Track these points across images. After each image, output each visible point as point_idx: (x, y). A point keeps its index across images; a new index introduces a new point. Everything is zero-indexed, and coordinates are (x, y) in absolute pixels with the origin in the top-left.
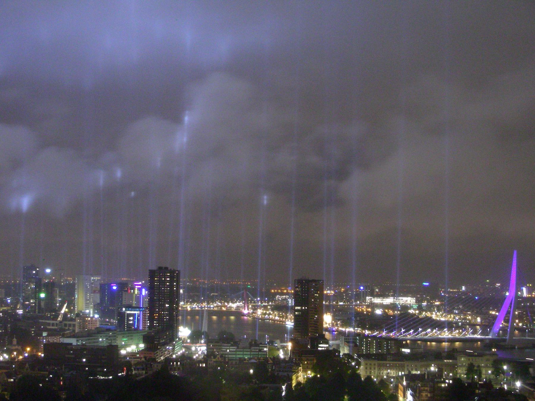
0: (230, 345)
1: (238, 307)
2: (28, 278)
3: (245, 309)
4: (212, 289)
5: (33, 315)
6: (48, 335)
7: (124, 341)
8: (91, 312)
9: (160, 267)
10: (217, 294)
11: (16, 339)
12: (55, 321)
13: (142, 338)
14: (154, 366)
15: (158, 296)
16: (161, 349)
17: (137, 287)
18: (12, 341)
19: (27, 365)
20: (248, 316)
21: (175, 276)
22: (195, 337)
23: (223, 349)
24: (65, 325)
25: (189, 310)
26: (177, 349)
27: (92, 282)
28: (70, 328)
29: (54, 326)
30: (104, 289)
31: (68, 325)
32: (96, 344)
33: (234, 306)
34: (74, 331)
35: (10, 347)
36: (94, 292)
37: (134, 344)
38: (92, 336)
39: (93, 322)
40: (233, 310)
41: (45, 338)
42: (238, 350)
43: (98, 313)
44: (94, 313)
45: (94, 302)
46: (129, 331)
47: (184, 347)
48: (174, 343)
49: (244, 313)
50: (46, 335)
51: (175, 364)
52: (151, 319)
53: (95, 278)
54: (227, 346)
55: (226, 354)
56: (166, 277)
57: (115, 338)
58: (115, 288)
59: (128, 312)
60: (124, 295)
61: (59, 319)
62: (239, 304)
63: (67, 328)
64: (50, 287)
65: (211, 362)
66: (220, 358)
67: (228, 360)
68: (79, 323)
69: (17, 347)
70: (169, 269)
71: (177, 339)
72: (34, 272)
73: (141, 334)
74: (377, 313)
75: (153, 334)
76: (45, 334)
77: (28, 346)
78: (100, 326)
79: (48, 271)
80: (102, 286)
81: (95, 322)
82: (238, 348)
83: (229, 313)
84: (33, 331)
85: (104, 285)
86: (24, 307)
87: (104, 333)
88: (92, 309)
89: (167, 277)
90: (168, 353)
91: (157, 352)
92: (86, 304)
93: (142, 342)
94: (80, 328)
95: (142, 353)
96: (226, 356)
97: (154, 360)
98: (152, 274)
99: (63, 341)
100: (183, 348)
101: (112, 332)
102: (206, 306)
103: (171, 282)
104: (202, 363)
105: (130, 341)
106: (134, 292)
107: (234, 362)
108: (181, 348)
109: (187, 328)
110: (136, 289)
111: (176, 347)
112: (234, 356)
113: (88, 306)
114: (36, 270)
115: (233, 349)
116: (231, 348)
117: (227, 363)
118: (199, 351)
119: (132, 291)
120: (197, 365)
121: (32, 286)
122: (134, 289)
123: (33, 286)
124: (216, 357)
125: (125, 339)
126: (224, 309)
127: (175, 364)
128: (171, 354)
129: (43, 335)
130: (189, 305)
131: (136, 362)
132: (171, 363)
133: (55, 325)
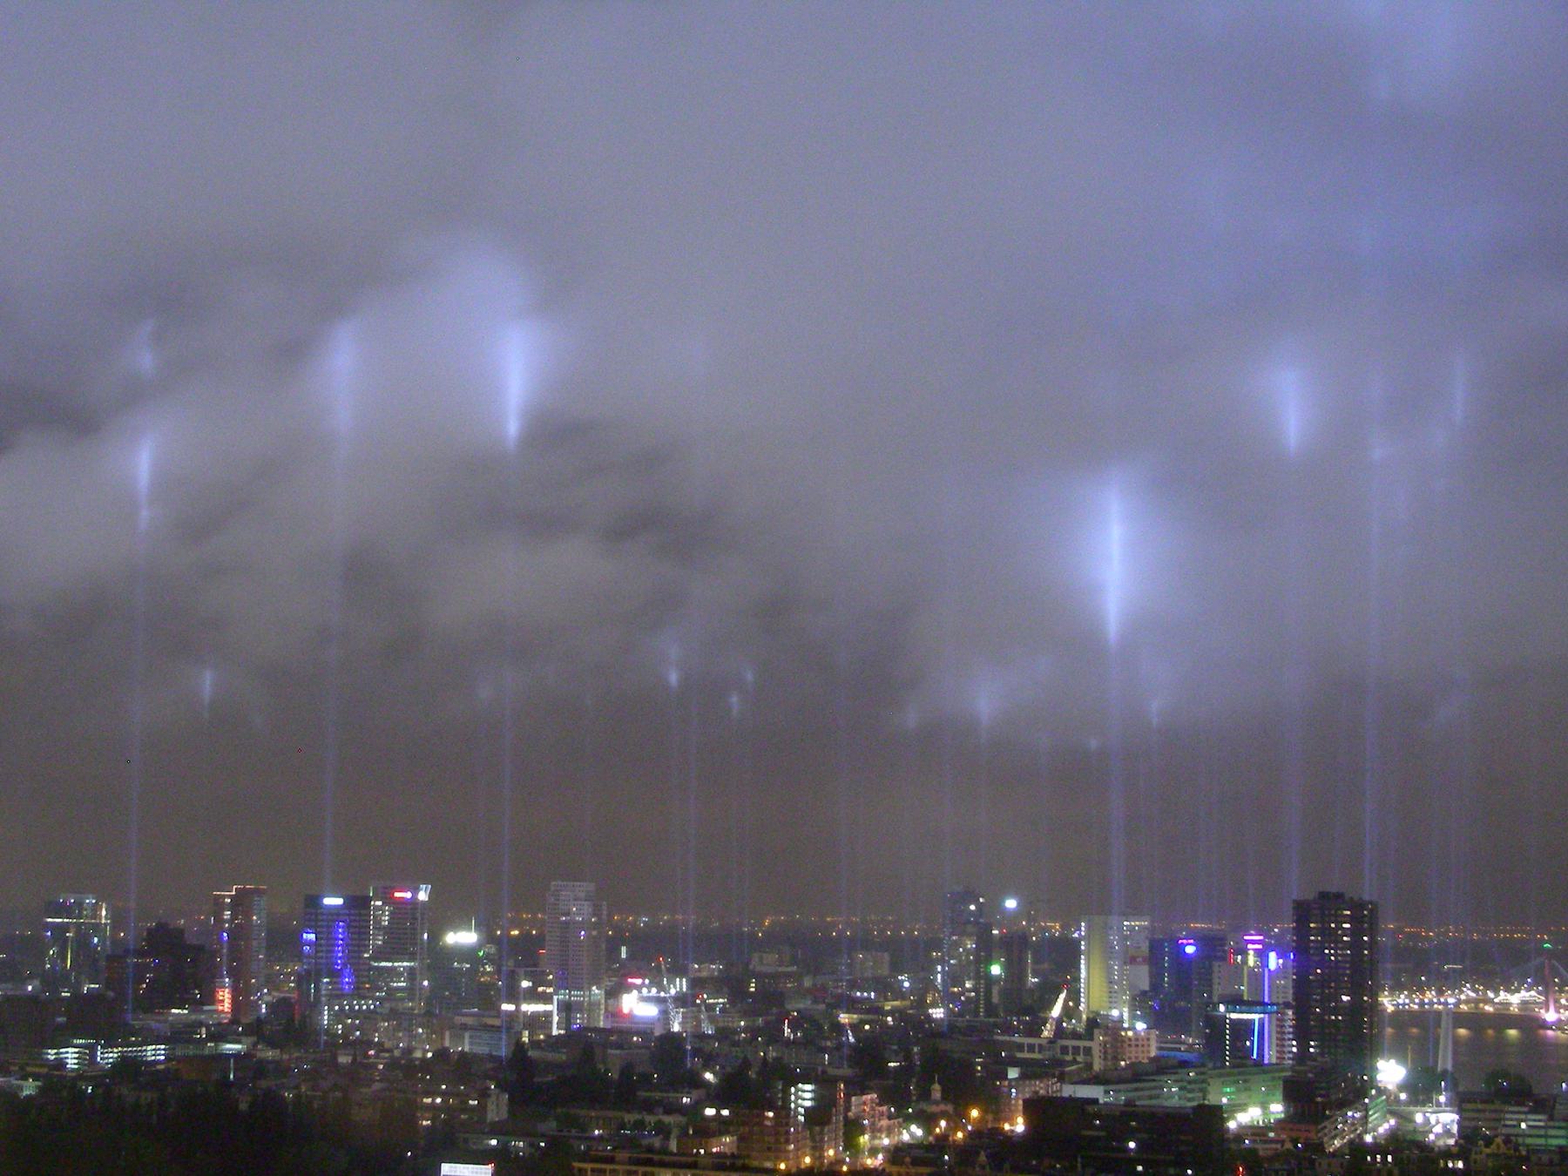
0: (1526, 1109)
1: (1524, 1003)
2: (960, 924)
3: (1547, 1010)
4: (1444, 953)
5: (974, 1021)
6: (1024, 1076)
7: (1225, 1094)
8: (1126, 1016)
9: (1323, 892)
10: (412, 964)
11: (939, 1083)
12: (1035, 1037)
13: (1281, 1086)
14: (1320, 1164)
15: (1341, 971)
16: (1332, 1120)
17: (1250, 946)
18: (930, 1091)
19: (982, 1158)
20: (1559, 1029)
21: (1364, 917)
22: (1421, 1088)
23: (1507, 1119)
24: (1064, 1050)
25: (1389, 1011)
26: (1375, 1119)
27: (1125, 933)
28: (1079, 1059)
29: (1074, 1047)
30: (1159, 951)
31: (1070, 1048)
32: (1154, 1102)
33: (1514, 999)
34: (1089, 1066)
35: (924, 1106)
36: (1132, 960)
37: (1255, 1104)
38: (1145, 1081)
39: (1140, 1043)
40: (1514, 1010)
41: (1013, 1083)
42: (1551, 1124)
43: (1142, 1018)
44: (1133, 1017)
45: (1131, 987)
46: (1238, 1067)
47: (1393, 1113)
48: (1367, 1101)
49: (1544, 1021)
50: (1017, 1076)
51: (1379, 1160)
52: (1302, 1034)
53: (1133, 924)
54: (1519, 1113)
55: (1516, 1136)
56: (1339, 919)
57: (1204, 1085)
58: (1190, 950)
59: (1234, 1016)
60: (1216, 969)
61: (1046, 1034)
62: (1528, 994)
63: (1069, 1058)
64: (1014, 947)
65: (1478, 1157)
66: (1502, 1145)
67: (1528, 1151)
68: (1103, 1045)
69: (942, 1107)
70: (1347, 897)
71: (1373, 1092)
72: (972, 907)
73: (1277, 1075)
74: (642, 1018)
75: (1310, 1075)
76: (1013, 1073)
77: (971, 1105)
78: (1158, 1052)
79: (1011, 904)
80: (1155, 947)
81: (1145, 1042)
82: (1551, 1118)
83: (1503, 1019)
84: (979, 1065)
85: (1160, 942)
86: (947, 998)
87: (1171, 1073)
88: (1127, 1006)
89: (1343, 919)
90: (1353, 1129)
91: (1325, 1127)
92: (1110, 992)
93: (1281, 1098)
94: (1105, 1059)
95: (1283, 1129)
96: (1520, 1140)
97: (1319, 1148)
98: (1303, 912)
99: (1074, 1092)
100: (1388, 1116)
101: (1198, 1070)
102: (1435, 1000)
103: (1356, 933)
104: (1455, 1157)
105: (1243, 1097)
106: (1245, 961)
107: (1545, 1158)
108: (1385, 1117)
109: (1392, 1061)
110: (1251, 952)
111: (1370, 1113)
112: (1542, 1141)
113: (1116, 997)
114: (976, 902)
115: (1539, 1120)
116: (1530, 1117)
117: (1526, 1160)
118: (1434, 1126)
119: (1239, 957)
120: (1442, 1163)
121: (969, 946)
122: (1244, 952)
123: (970, 945)
124: (1491, 1144)
125: (1228, 1090)
126: (1489, 1009)
127: (1379, 1160)
128: (1358, 1132)
129: (1010, 1077)
130: (1386, 996)
131: (1269, 1153)
132: (1369, 1158)
133: (1082, 1050)
